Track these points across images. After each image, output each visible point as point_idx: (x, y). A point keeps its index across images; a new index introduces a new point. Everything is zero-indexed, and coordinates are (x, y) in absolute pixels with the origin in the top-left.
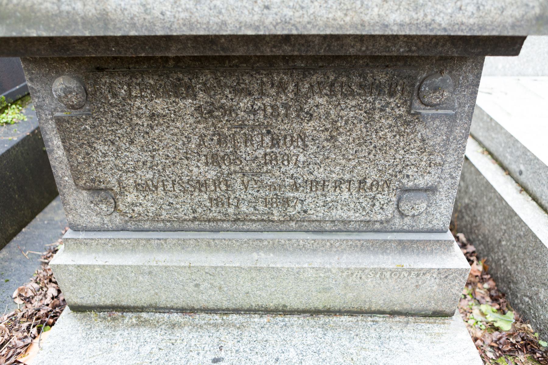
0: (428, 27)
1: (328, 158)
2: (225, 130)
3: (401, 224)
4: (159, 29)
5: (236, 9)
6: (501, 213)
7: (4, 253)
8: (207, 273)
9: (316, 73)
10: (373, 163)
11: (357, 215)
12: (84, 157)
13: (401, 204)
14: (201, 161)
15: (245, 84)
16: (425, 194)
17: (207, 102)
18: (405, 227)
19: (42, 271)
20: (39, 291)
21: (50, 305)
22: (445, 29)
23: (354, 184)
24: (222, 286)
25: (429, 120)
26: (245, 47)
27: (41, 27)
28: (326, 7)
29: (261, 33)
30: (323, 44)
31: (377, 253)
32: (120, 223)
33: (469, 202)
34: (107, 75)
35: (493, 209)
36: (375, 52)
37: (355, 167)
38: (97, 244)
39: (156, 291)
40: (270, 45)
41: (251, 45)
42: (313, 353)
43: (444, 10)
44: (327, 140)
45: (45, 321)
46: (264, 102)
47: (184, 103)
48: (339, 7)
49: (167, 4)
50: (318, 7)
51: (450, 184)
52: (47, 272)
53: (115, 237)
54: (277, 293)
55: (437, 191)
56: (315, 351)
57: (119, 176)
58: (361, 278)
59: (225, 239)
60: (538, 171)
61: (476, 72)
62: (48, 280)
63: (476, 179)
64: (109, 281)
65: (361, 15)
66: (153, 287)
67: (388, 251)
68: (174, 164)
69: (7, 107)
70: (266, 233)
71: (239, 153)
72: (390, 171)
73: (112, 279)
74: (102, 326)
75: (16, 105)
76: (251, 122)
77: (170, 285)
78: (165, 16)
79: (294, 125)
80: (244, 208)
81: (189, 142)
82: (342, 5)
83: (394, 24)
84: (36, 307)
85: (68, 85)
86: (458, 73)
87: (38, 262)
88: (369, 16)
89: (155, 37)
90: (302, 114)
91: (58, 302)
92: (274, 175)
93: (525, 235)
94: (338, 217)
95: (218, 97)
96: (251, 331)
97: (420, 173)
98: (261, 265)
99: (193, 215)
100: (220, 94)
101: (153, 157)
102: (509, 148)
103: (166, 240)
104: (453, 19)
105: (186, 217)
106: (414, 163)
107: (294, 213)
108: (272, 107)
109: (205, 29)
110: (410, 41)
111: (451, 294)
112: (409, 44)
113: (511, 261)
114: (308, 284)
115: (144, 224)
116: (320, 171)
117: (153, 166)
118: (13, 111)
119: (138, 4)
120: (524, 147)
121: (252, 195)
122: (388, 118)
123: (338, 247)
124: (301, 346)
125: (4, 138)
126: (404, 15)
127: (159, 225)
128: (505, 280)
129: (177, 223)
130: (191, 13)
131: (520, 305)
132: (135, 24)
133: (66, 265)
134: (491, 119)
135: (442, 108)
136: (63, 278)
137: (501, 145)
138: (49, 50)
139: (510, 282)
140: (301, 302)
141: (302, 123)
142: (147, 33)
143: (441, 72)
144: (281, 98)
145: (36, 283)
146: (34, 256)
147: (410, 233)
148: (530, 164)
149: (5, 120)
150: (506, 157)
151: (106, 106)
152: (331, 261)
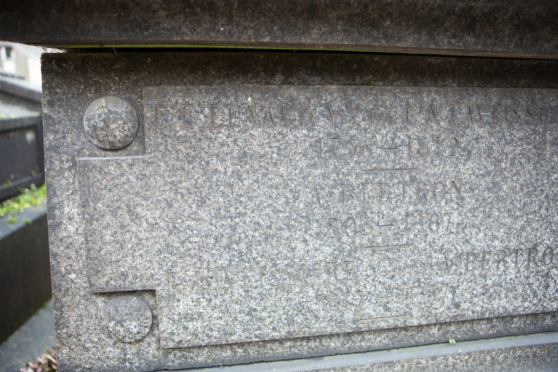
1: (489, 216)
2: (352, 179)
10: (545, 221)
11: (527, 304)
12: (116, 233)
15: (386, 107)
17: (329, 134)
23: (522, 255)
30: (514, 36)
32: (155, 357)
34: (181, 92)
37: (523, 228)
40: (449, 33)
41: (425, 33)
44: (489, 189)
47: (295, 136)
57: (170, 264)
68: (266, 238)
70: (395, 350)
71: (369, 215)
76: (390, 165)
79: (447, 168)
80: (369, 309)
81: (296, 199)
85: (113, 109)
92: (416, 248)
94: (501, 310)
95: (345, 126)
100: (350, 120)
101: (234, 228)
107: (442, 309)
115: (197, 356)
121: (383, 284)
123: (503, 361)
127: (224, 354)
138: (114, 29)
144: (432, 127)
151: (170, 141)
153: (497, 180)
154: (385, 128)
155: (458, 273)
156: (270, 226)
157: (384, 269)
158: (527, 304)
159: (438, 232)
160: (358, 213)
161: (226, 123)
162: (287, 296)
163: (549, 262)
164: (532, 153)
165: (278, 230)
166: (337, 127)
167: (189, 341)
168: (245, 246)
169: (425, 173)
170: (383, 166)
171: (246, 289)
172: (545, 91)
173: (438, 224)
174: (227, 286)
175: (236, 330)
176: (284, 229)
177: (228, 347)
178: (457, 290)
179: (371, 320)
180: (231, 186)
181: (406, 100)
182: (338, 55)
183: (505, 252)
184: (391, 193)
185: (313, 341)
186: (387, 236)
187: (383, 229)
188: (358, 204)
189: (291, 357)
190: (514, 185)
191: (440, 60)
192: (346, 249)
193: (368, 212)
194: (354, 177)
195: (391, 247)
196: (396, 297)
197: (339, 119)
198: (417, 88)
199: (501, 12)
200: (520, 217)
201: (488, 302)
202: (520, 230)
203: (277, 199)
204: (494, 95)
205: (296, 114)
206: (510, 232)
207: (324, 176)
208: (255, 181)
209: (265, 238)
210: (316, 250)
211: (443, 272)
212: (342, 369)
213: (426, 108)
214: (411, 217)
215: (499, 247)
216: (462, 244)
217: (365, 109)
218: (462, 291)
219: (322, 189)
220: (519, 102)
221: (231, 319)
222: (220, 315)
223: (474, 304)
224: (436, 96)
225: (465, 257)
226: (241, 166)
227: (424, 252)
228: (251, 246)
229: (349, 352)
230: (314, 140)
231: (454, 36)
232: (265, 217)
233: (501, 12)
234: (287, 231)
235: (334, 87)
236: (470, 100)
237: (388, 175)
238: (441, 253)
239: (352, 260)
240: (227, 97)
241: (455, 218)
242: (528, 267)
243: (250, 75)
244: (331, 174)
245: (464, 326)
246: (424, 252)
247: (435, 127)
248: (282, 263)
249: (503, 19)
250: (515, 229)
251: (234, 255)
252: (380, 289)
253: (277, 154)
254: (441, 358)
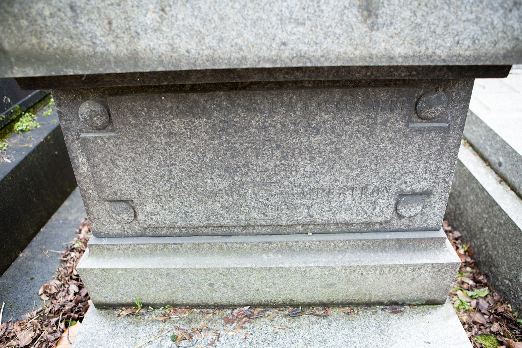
0: (430, 58)
1: (333, 168)
2: (238, 146)
3: (399, 224)
4: (184, 65)
5: (256, 46)
6: (483, 203)
7: (27, 252)
8: (220, 274)
11: (359, 218)
12: (107, 173)
16: (420, 198)
18: (402, 227)
19: (62, 269)
20: (61, 287)
21: (73, 301)
22: (444, 60)
24: (235, 285)
25: (426, 133)
26: (259, 75)
27: (78, 66)
28: (338, 43)
29: (278, 66)
31: (377, 251)
33: (453, 191)
35: (475, 199)
36: (379, 77)
37: (358, 175)
38: (119, 249)
39: (174, 290)
40: (283, 72)
42: (319, 343)
43: (444, 44)
44: (333, 152)
45: (71, 316)
46: (275, 119)
48: (349, 43)
49: (192, 43)
50: (331, 42)
52: (67, 270)
53: (134, 243)
54: (285, 290)
55: (431, 194)
56: (322, 341)
57: (138, 188)
58: (362, 274)
59: (236, 243)
60: (516, 163)
61: (467, 89)
62: (69, 277)
63: (459, 170)
64: (130, 282)
65: (369, 49)
66: (171, 287)
67: (387, 249)
68: (189, 177)
69: (21, 116)
73: (133, 280)
74: (125, 322)
75: (29, 112)
77: (187, 285)
78: (190, 54)
79: (302, 139)
80: (254, 215)
81: (204, 157)
82: (353, 41)
83: (399, 56)
84: (61, 303)
86: (451, 90)
87: (57, 260)
88: (376, 50)
89: (181, 71)
91: (80, 298)
93: (505, 224)
94: (341, 220)
96: (262, 324)
97: (417, 179)
98: (271, 266)
99: (207, 222)
101: (170, 171)
102: (489, 140)
103: (181, 244)
104: (451, 52)
105: (201, 224)
107: (301, 218)
109: (226, 64)
111: (443, 285)
113: (493, 247)
114: (314, 281)
116: (325, 180)
117: (170, 179)
118: (26, 118)
119: (166, 44)
120: (503, 141)
121: (262, 202)
124: (309, 337)
125: (21, 146)
126: (408, 49)
127: (175, 231)
128: (487, 264)
129: (192, 229)
130: (215, 50)
131: (501, 287)
132: (162, 61)
133: (91, 269)
135: (436, 122)
136: (89, 280)
137: (481, 138)
139: (491, 266)
140: (307, 297)
141: (309, 138)
142: (173, 69)
143: (436, 90)
144: (290, 115)
145: (58, 280)
146: (54, 255)
148: (509, 157)
149: (20, 128)
152: (335, 260)
241: (309, 168)
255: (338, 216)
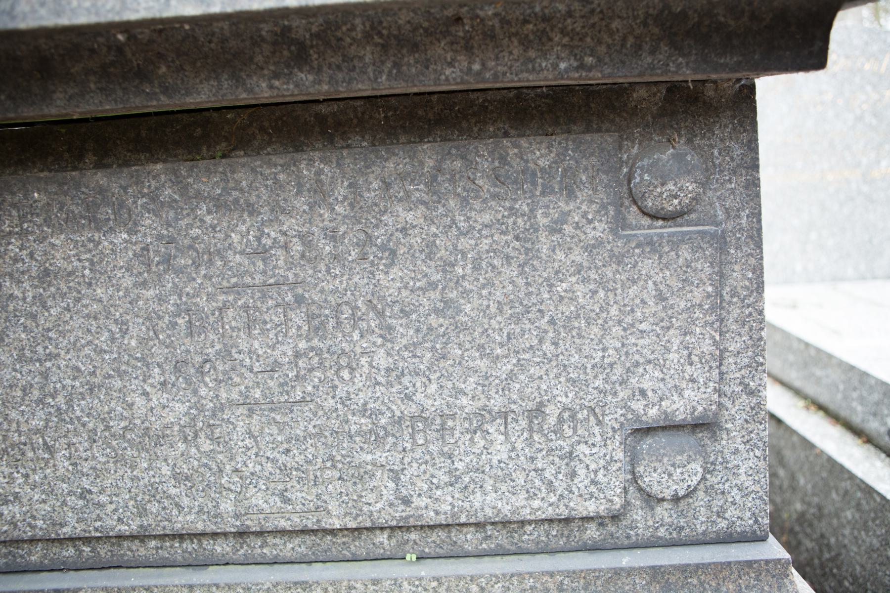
1: (444, 357)
2: (202, 301)
6: (877, 522)
9: (394, 154)
10: (554, 363)
11: (536, 503)
13: (641, 469)
14: (151, 381)
15: (242, 190)
18: (662, 532)
23: (517, 421)
25: (666, 249)
30: (383, 62)
35: (857, 516)
37: (511, 376)
40: (266, 72)
41: (226, 76)
44: (437, 312)
46: (285, 228)
47: (111, 242)
51: (748, 409)
55: (721, 429)
61: (744, 137)
68: (91, 390)
70: (320, 564)
71: (236, 356)
72: (597, 383)
76: (258, 279)
79: (356, 279)
80: (258, 500)
90: (371, 250)
92: (321, 407)
94: (489, 512)
95: (183, 223)
100: (188, 215)
101: (45, 375)
102: (855, 389)
105: (124, 528)
106: (652, 357)
108: (301, 237)
109: (88, 10)
110: (576, 43)
112: (576, 51)
115: (30, 553)
121: (274, 461)
122: (570, 249)
127: (65, 553)
134: (807, 345)
141: (372, 273)
144: (321, 215)
147: (675, 548)
150: (853, 410)
153: (451, 295)
154: (244, 222)
155: (401, 449)
156: (94, 372)
157: (272, 438)
158: (536, 503)
159: (354, 383)
160: (218, 353)
161: (17, 230)
162: (132, 472)
163: (571, 434)
164: (513, 248)
165: (105, 378)
166: (171, 226)
167: (6, 532)
168: (63, 401)
169: (318, 289)
170: (248, 280)
171: (73, 461)
172: (523, 142)
173: (352, 370)
174: (46, 456)
175: (68, 519)
176: (113, 377)
177: (70, 544)
178: (402, 476)
179: (263, 516)
180: (34, 317)
181: (272, 176)
182: (171, 117)
183: (482, 415)
184: (265, 323)
185: (188, 541)
186: (269, 388)
187: (260, 377)
188: (216, 340)
189: (160, 563)
190: (485, 303)
191: (335, 107)
192: (208, 407)
193: (234, 351)
194: (205, 299)
195: (278, 405)
196: (299, 483)
197: (172, 214)
198: (289, 156)
199: (344, 28)
200: (503, 356)
201: (462, 498)
202: (506, 379)
203: (97, 333)
204: (428, 155)
205: (110, 211)
206: (487, 383)
207: (159, 300)
208: (65, 309)
209: (90, 389)
210: (164, 407)
211: (372, 447)
212: (229, 587)
213: (308, 185)
214: (305, 359)
215: (470, 407)
216: (399, 403)
217: (209, 196)
218: (411, 478)
219: (160, 318)
220: (477, 163)
221: (59, 504)
222: (43, 497)
223: (436, 499)
224: (322, 166)
225: (408, 423)
226: (44, 289)
227: (334, 415)
228: (72, 400)
229: (246, 562)
230: (137, 248)
231: (276, 76)
232: (84, 360)
233: (344, 28)
234: (117, 379)
235: (159, 166)
236: (384, 167)
237: (258, 295)
238: (364, 415)
239: (218, 423)
240: (13, 194)
241: (382, 360)
242: (530, 442)
243: (50, 159)
244: (170, 295)
245: (434, 534)
246: (334, 415)
247: (326, 216)
248: (118, 426)
249: (353, 39)
250: (497, 377)
251: (50, 413)
252: (270, 469)
253: (90, 270)
254: (389, 582)
255: (477, 499)
